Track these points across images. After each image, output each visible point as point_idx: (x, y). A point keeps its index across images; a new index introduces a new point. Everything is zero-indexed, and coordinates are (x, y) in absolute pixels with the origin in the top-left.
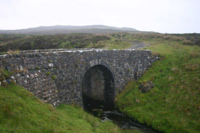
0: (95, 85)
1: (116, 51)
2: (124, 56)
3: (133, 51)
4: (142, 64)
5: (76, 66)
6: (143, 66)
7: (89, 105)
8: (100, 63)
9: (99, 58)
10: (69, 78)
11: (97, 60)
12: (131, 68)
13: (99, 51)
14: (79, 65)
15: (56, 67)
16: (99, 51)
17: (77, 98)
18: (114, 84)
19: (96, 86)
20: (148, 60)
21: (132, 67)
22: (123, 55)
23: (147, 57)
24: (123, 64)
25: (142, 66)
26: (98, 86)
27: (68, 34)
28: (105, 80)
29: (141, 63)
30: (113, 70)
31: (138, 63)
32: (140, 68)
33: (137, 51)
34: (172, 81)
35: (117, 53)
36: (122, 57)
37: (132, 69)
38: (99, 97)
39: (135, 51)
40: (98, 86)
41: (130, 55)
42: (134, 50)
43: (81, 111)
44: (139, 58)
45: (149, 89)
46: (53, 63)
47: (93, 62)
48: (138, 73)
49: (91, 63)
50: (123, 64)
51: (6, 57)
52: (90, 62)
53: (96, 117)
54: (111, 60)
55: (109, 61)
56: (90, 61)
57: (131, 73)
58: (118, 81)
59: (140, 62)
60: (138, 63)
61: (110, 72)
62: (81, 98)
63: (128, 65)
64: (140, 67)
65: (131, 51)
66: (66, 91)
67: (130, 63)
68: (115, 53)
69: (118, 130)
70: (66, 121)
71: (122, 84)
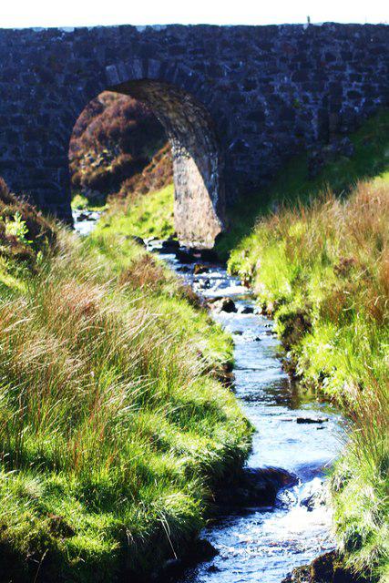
2: (273, 50)
4: (359, 80)
7: (172, 579)
10: (14, 115)
12: (306, 100)
21: (308, 94)
24: (266, 81)
25: (359, 90)
32: (350, 98)
34: (9, 438)
41: (303, 46)
47: (120, 66)
49: (112, 70)
50: (266, 81)
52: (108, 68)
54: (207, 63)
56: (107, 64)
57: (308, 117)
59: (349, 71)
60: (343, 78)
63: (293, 84)
69: (342, 203)
70: (189, 416)
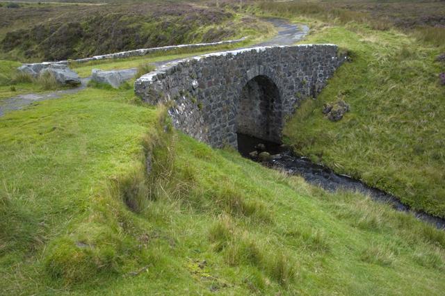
0: (241, 107)
1: (285, 48)
3: (311, 47)
5: (228, 81)
6: (325, 73)
8: (261, 73)
9: (259, 63)
11: (257, 67)
13: (260, 50)
14: (232, 79)
15: (201, 85)
16: (260, 50)
17: (231, 137)
18: (280, 107)
19: (244, 109)
20: (333, 62)
22: (295, 56)
23: (330, 57)
26: (247, 109)
27: (135, 59)
28: (261, 99)
29: (322, 68)
30: (279, 83)
31: (317, 69)
33: (315, 48)
35: (286, 52)
36: (293, 59)
37: (306, 79)
38: (249, 127)
39: (312, 47)
40: (247, 109)
41: (306, 55)
42: (311, 45)
43: (237, 156)
44: (319, 59)
45: (341, 115)
46: (198, 78)
48: (317, 86)
51: (155, 79)
53: (245, 157)
55: (275, 67)
58: (286, 102)
61: (275, 85)
62: (235, 135)
64: (321, 76)
65: (258, 51)
66: (216, 127)
67: (305, 69)
68: (283, 52)
71: (293, 106)
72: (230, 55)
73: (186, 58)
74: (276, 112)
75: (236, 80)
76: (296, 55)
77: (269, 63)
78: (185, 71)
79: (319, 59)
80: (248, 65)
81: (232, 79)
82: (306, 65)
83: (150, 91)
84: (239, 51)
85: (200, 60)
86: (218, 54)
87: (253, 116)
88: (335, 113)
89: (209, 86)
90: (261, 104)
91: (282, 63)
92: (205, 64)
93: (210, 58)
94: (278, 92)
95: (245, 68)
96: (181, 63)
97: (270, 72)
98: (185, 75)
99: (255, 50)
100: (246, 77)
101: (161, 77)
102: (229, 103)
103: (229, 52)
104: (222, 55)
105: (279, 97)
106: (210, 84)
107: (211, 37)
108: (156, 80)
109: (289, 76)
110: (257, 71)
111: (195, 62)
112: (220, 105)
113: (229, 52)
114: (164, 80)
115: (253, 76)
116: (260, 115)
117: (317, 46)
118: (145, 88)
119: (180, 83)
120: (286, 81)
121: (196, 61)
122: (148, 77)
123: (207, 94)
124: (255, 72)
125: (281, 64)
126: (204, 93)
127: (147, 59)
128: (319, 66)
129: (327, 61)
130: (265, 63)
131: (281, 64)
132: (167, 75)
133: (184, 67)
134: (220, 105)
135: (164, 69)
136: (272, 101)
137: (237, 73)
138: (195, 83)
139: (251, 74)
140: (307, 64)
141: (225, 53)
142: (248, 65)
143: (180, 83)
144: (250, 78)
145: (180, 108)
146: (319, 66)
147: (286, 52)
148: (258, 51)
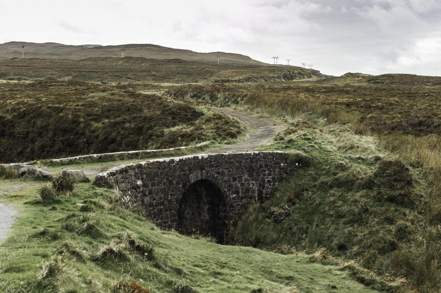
0: (191, 213)
5: (171, 183)
8: (204, 178)
9: (202, 169)
13: (203, 157)
14: (174, 182)
15: (144, 185)
16: (203, 157)
31: (265, 175)
37: (254, 186)
39: (259, 154)
41: (252, 162)
42: (257, 152)
48: (264, 191)
65: (200, 158)
67: (251, 175)
72: (173, 161)
73: (132, 163)
74: (222, 216)
75: (178, 183)
76: (242, 162)
77: (212, 169)
78: (132, 172)
79: (266, 166)
80: (190, 170)
81: (174, 182)
82: (251, 171)
83: (105, 182)
84: (181, 158)
85: (145, 164)
86: (161, 160)
87: (202, 221)
88: (277, 216)
89: (152, 187)
90: (208, 209)
91: (226, 168)
92: (149, 168)
93: (153, 163)
94: (223, 195)
95: (187, 172)
96: (129, 166)
97: (213, 177)
98: (131, 175)
99: (198, 157)
100: (189, 181)
101: (112, 174)
102: (171, 203)
103: (172, 158)
104: (165, 161)
105: (224, 201)
106: (153, 185)
107: (173, 141)
108: (109, 176)
109: (234, 181)
110: (200, 176)
111: (140, 166)
112: (162, 204)
113: (172, 158)
114: (115, 177)
115: (196, 180)
116: (208, 220)
117: (264, 153)
118: (102, 180)
119: (127, 181)
120: (231, 186)
121: (141, 165)
122: (105, 174)
123: (150, 193)
124: (197, 176)
125: (225, 170)
126: (147, 192)
127: (102, 175)
128: (267, 172)
129: (275, 167)
130: (208, 169)
131: (225, 170)
132: (117, 173)
133: (131, 169)
134: (162, 204)
135: (115, 169)
136: (218, 205)
137: (179, 176)
138: (139, 183)
139: (193, 178)
140: (253, 170)
141: (167, 159)
142: (190, 170)
143: (127, 181)
144: (193, 181)
145: (125, 198)
146: (267, 172)
147: (231, 159)
148: (200, 158)
